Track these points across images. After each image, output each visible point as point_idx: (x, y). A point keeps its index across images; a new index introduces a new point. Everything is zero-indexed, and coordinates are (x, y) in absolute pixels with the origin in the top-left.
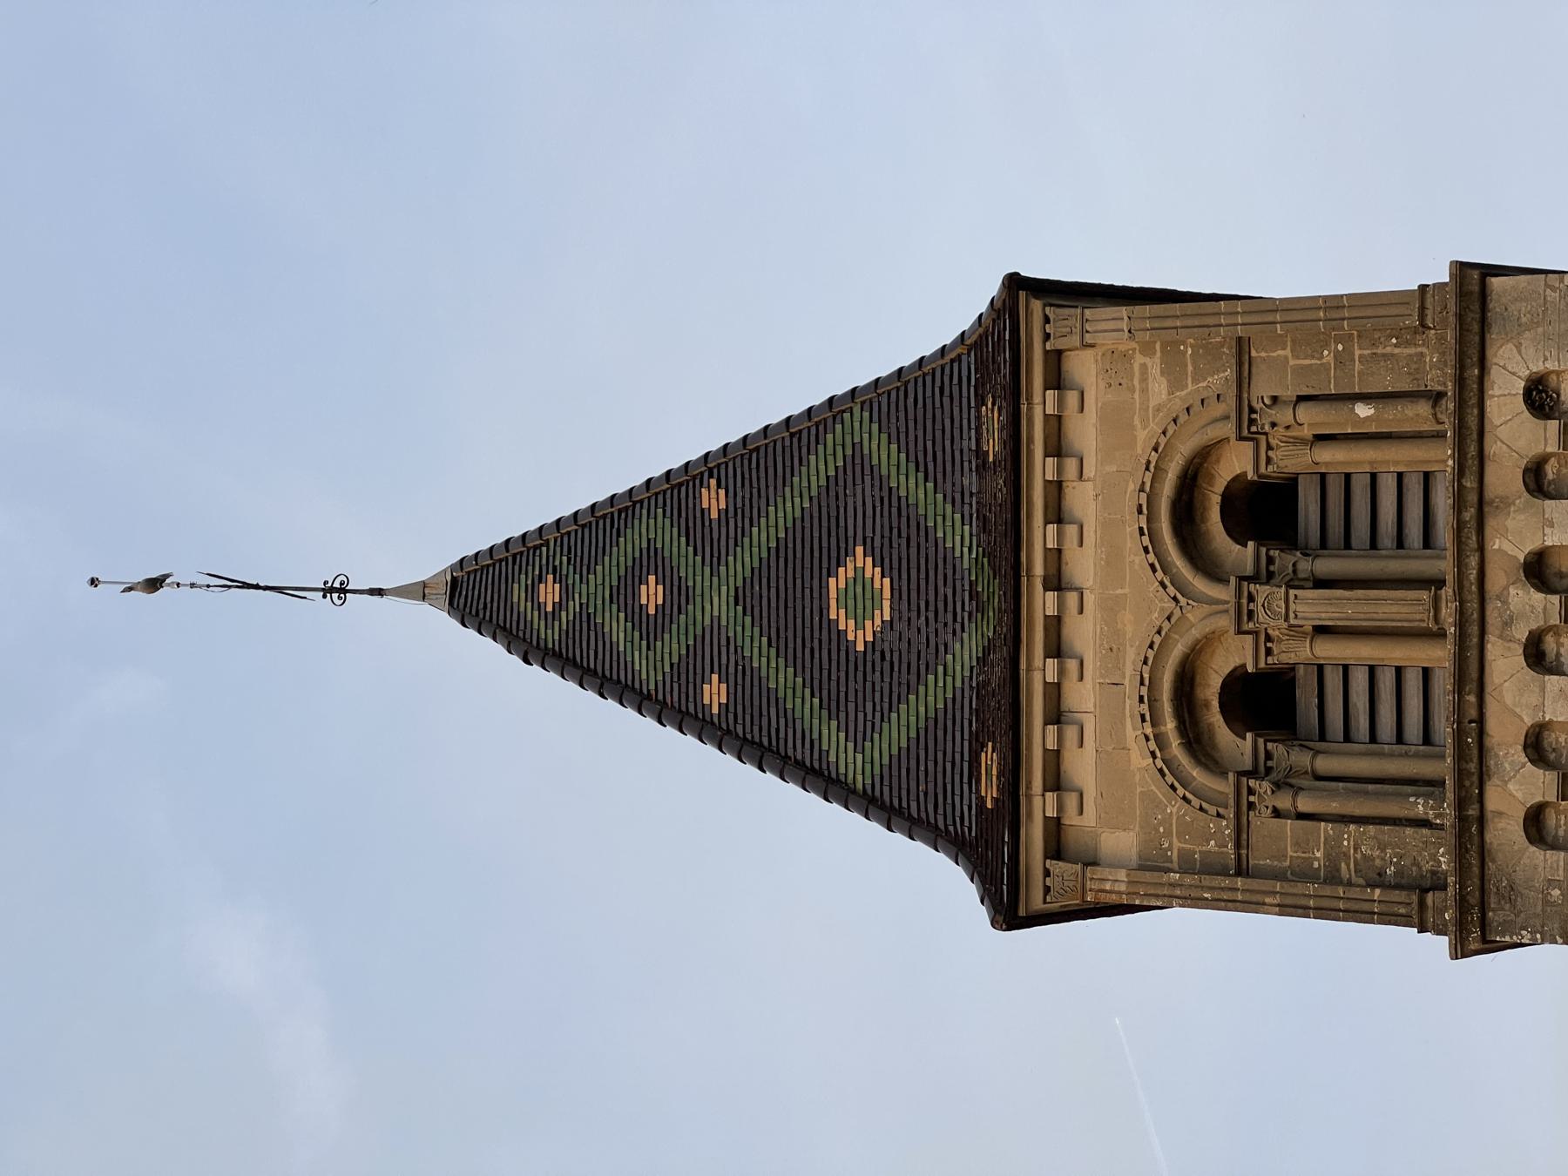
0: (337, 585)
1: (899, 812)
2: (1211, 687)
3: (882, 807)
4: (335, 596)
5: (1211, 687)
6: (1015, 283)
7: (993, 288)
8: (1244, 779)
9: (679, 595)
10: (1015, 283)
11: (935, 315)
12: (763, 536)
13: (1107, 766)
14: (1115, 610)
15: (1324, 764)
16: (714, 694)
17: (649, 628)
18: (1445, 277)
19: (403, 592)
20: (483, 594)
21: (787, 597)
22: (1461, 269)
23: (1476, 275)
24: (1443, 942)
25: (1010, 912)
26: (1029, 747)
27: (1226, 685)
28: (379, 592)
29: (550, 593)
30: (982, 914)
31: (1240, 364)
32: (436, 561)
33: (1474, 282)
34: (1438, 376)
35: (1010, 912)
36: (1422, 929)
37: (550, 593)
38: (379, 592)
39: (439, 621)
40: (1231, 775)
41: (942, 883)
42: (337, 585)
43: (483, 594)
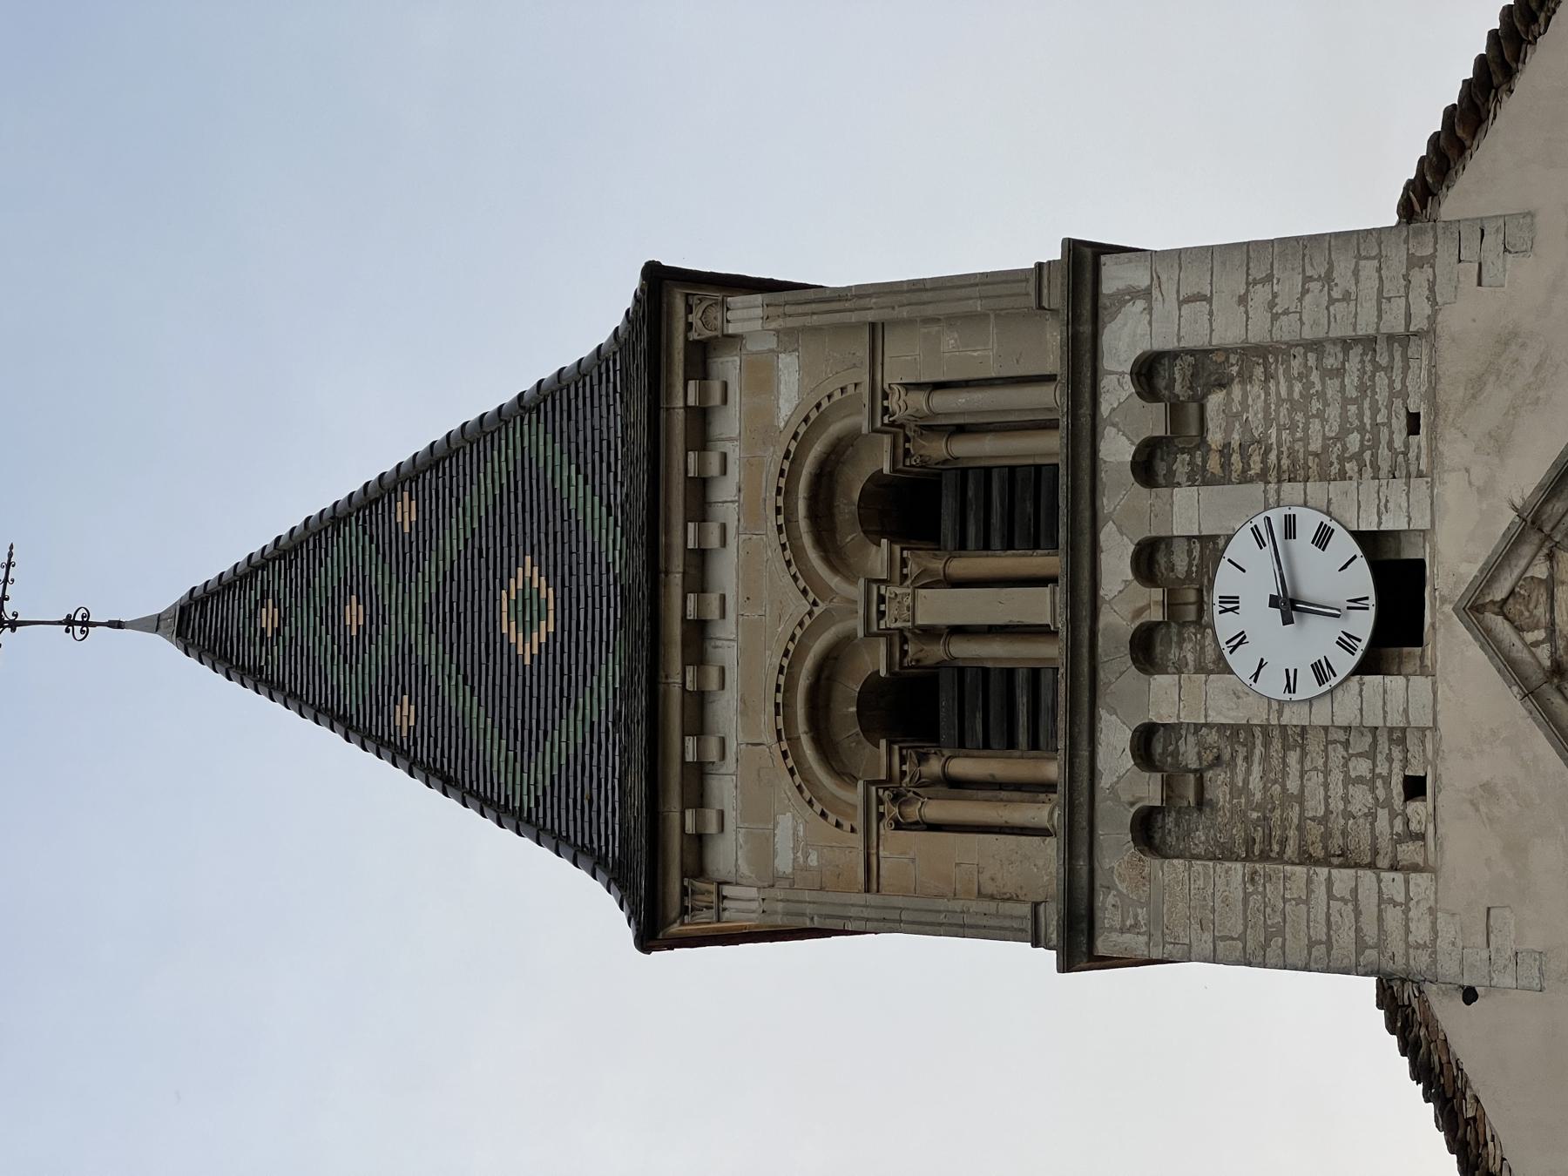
0: (79, 618)
1: (281, 687)
2: (849, 688)
3: (477, 796)
4: (78, 628)
5: (849, 688)
6: (657, 278)
7: (634, 282)
8: (873, 789)
9: (376, 616)
10: (657, 278)
11: (584, 317)
12: (451, 543)
13: (760, 811)
14: (758, 603)
15: (963, 767)
16: (405, 715)
17: (348, 653)
18: (1056, 254)
19: (140, 625)
20: (212, 625)
21: (463, 615)
22: (1074, 248)
23: (1088, 252)
24: (1050, 957)
25: (650, 937)
26: (668, 466)
27: (861, 702)
28: (118, 625)
29: (268, 618)
30: (628, 934)
31: (1074, 319)
32: (167, 596)
33: (1084, 259)
34: (1052, 362)
35: (650, 937)
36: (1035, 944)
37: (268, 618)
38: (118, 625)
39: (165, 650)
40: (860, 784)
41: (592, 908)
42: (79, 618)
43: (212, 625)
